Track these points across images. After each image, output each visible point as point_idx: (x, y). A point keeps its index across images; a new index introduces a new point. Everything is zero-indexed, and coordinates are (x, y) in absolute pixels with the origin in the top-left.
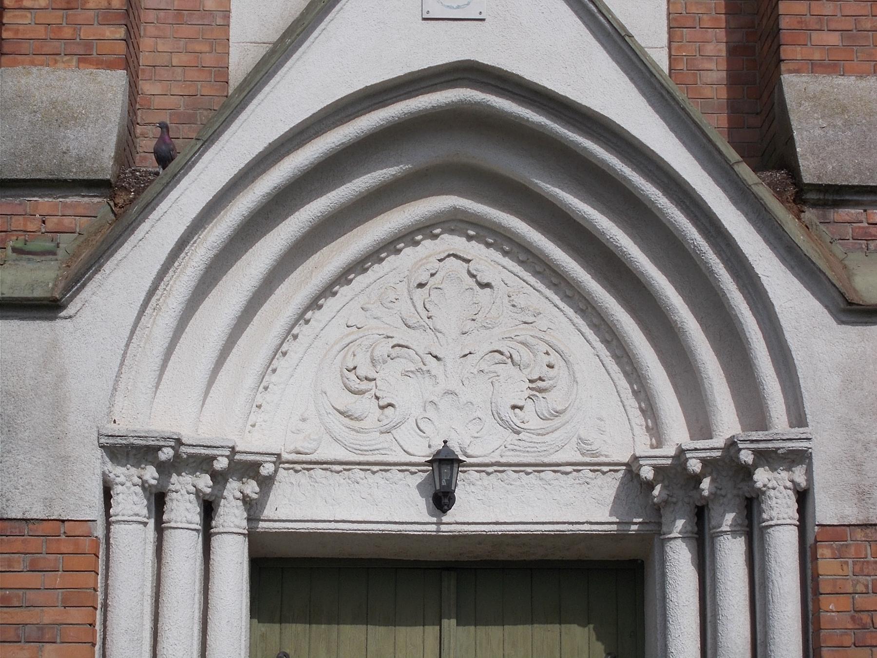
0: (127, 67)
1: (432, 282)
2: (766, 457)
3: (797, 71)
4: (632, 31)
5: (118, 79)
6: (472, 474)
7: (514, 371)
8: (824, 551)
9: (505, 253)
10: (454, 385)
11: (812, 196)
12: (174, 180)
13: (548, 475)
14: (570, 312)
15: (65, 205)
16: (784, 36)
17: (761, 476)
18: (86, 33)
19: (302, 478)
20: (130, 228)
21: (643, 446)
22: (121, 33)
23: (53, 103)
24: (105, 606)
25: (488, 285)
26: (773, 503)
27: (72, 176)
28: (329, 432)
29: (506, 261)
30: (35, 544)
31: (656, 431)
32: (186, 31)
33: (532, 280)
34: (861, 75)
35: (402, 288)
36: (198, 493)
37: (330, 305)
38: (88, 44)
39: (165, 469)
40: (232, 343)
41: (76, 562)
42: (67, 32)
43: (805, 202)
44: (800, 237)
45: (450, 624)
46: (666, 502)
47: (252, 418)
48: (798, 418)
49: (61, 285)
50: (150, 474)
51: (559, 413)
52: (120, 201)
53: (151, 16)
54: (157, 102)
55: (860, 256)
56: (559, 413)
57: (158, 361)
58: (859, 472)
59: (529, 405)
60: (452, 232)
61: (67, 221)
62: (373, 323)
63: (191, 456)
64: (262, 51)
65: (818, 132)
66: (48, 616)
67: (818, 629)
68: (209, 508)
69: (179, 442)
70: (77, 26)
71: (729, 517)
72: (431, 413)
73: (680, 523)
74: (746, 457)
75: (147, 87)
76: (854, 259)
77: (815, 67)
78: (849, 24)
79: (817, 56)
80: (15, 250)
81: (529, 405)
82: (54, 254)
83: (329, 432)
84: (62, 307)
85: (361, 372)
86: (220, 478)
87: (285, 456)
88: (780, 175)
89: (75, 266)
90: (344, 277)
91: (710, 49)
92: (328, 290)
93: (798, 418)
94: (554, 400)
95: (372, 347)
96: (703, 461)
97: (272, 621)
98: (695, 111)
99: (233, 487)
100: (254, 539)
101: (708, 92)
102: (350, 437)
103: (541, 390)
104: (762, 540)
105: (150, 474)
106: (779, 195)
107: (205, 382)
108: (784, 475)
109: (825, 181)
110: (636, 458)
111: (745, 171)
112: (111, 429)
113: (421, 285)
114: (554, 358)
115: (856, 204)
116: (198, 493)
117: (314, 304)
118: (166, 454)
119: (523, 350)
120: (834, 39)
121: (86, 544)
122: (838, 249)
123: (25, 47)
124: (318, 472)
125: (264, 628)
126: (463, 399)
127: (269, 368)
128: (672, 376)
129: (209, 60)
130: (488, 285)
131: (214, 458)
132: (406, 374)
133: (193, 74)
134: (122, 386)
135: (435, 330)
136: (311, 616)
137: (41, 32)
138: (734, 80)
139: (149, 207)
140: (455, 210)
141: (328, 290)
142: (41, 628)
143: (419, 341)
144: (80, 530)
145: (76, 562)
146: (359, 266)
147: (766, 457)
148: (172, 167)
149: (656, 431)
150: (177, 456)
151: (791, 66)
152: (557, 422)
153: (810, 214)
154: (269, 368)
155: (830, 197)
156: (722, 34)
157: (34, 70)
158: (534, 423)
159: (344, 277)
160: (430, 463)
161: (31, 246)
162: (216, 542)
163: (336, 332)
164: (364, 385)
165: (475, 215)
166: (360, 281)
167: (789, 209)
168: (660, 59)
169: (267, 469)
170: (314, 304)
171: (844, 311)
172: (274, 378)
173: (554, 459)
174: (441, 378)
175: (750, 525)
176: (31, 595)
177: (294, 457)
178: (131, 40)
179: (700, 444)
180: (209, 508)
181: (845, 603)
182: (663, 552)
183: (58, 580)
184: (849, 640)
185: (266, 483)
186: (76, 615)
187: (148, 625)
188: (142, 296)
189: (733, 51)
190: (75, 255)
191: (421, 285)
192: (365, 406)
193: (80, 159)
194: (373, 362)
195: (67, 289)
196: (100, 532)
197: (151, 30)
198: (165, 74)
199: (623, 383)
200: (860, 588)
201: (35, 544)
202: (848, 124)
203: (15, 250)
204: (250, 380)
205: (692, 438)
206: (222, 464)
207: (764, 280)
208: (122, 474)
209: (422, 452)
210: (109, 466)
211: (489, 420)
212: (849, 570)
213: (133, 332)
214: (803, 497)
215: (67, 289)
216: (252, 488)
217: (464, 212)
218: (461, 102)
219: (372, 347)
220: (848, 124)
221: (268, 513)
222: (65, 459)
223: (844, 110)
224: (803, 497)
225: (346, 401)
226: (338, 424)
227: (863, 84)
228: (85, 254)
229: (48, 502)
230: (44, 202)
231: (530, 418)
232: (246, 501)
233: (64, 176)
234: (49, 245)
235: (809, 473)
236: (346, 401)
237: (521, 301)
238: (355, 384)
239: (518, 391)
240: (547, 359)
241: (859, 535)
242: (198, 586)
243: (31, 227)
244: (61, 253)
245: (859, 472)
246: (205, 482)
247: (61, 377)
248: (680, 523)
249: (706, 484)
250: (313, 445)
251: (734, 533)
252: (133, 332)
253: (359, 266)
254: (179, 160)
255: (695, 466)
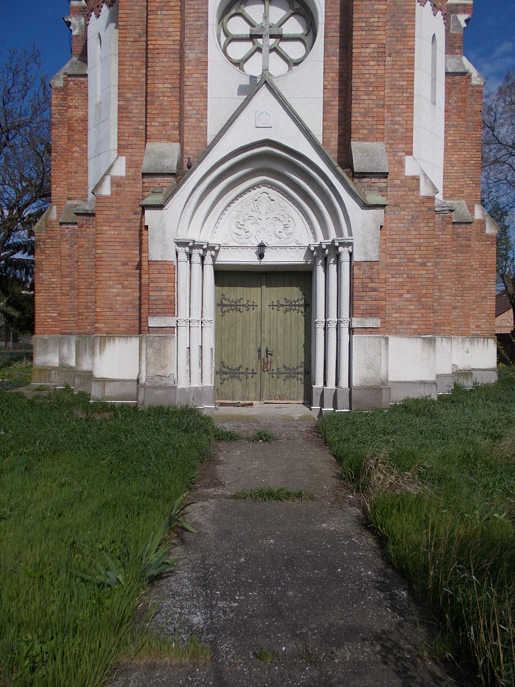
0: (180, 142)
1: (259, 199)
2: (341, 244)
3: (355, 141)
4: (311, 130)
5: (178, 145)
6: (269, 249)
7: (280, 223)
8: (355, 268)
9: (278, 192)
10: (264, 226)
11: (356, 175)
12: (191, 173)
13: (288, 249)
14: (294, 207)
15: (164, 180)
16: (352, 131)
17: (340, 249)
18: (168, 133)
19: (226, 250)
20: (180, 186)
21: (312, 242)
22: (178, 132)
23: (161, 152)
24: (177, 282)
25: (273, 200)
26: (343, 256)
27: (165, 172)
28: (233, 239)
29: (278, 194)
30: (159, 267)
31: (315, 238)
32: (196, 132)
33: (285, 199)
34: (372, 142)
35: (251, 201)
36: (199, 254)
37: (233, 205)
38: (169, 136)
39: (191, 248)
40: (482, 201)
41: (169, 271)
42: (164, 132)
43: (355, 177)
44: (353, 187)
45: (264, 287)
46: (317, 256)
47: (213, 235)
48: (350, 234)
49: (164, 201)
50: (187, 249)
51: (291, 233)
52: (178, 178)
53: (186, 128)
54: (189, 152)
55: (368, 191)
56: (291, 233)
57: (189, 220)
58: (365, 248)
59: (283, 231)
60: (264, 186)
61: (165, 184)
62: (244, 210)
63: (197, 245)
64: (214, 137)
65: (360, 157)
66: (163, 285)
67: (353, 287)
68: (203, 258)
69: (194, 241)
70: (166, 130)
71: (333, 260)
72: (258, 234)
73: (320, 261)
74: (337, 244)
75: (186, 148)
76: (367, 192)
77: (360, 139)
78: (370, 127)
79: (361, 136)
80: (152, 192)
81: (283, 231)
82: (161, 193)
83: (233, 239)
84: (164, 207)
85: (241, 223)
86: (205, 250)
87: (222, 245)
88: (348, 170)
89: (167, 196)
90: (236, 198)
91: (333, 135)
92: (232, 202)
93: (350, 234)
94: (290, 230)
95: (244, 217)
96: (314, 247)
97: (220, 286)
98: (327, 152)
99: (209, 252)
100: (214, 265)
101: (332, 147)
102: (238, 240)
103: (286, 228)
104: (340, 265)
105: (187, 249)
106: (348, 175)
107: (201, 227)
108: (346, 248)
109: (360, 171)
110: (310, 245)
111: (339, 169)
112: (177, 238)
113: (256, 200)
114: (290, 219)
115: (368, 177)
116: (199, 254)
117: (229, 205)
118: (191, 244)
119: (282, 217)
120: (366, 131)
121: (172, 267)
122: (363, 190)
123: (153, 137)
124: (230, 249)
125: (218, 288)
126: (267, 230)
127: (217, 222)
128: (320, 224)
129: (202, 140)
130: (273, 200)
131: (203, 245)
132: (252, 224)
133: (198, 144)
134: (180, 227)
135: (260, 212)
136: (230, 285)
137: (157, 132)
138: (339, 144)
139: (185, 180)
140: (265, 180)
141: (232, 202)
142: (161, 288)
143: (255, 215)
144: (170, 263)
145: (169, 271)
146: (240, 195)
147: (341, 244)
148: (191, 169)
149: (315, 238)
150: (194, 244)
151: (355, 139)
152: (291, 236)
153: (356, 180)
154: (217, 222)
155: (361, 176)
156: (337, 131)
157: (156, 143)
158: (285, 236)
159: (236, 198)
160: (258, 246)
161: (156, 191)
162: (204, 266)
163: (234, 213)
164: (242, 227)
165: (270, 181)
166: (240, 199)
167: (350, 179)
168: (320, 139)
169: (217, 248)
170: (229, 205)
171: (363, 206)
172: (219, 225)
173: (289, 245)
174: (261, 225)
175: (338, 262)
176: (333, 268)
177: (224, 245)
178: (181, 134)
179: (325, 241)
180: (203, 258)
181: (360, 281)
182: (316, 269)
183: (165, 276)
184: (361, 290)
185: (217, 252)
186: (170, 284)
187: (188, 287)
188: (184, 204)
189: (339, 136)
190: (167, 193)
191: (256, 200)
192: (242, 232)
193: (167, 167)
194: (244, 221)
195: (165, 202)
196: (175, 264)
197: (187, 132)
198: (190, 144)
199: (307, 225)
200: (364, 277)
201: (159, 267)
202: (368, 155)
203: (152, 192)
204: (213, 226)
205: (324, 239)
206: (205, 247)
207: (343, 198)
208: (181, 250)
209: (256, 244)
210: (177, 247)
211: (273, 236)
212: (361, 273)
213: (182, 213)
214: (351, 254)
215: (165, 202)
216: (213, 253)
217: (267, 180)
218: (266, 151)
219: (244, 217)
220: (368, 155)
221: (218, 259)
222: (166, 245)
223: (367, 151)
224: (351, 254)
225: (237, 231)
226: (235, 236)
227: (373, 144)
228: (170, 192)
229: (162, 256)
230: (159, 179)
231: (284, 235)
232: (212, 256)
233: (163, 172)
234: (161, 191)
235: (353, 248)
236: (237, 231)
237: (282, 204)
238: (239, 226)
239: (280, 228)
240: (288, 220)
241: (364, 264)
242: (201, 277)
243: (156, 186)
244: (163, 192)
245: (365, 248)
246: (201, 251)
247: (164, 225)
248: (320, 261)
249: (327, 251)
250: (228, 242)
251: (334, 264)
252: (182, 213)
253: (240, 195)
254: (192, 167)
255: (324, 247)
